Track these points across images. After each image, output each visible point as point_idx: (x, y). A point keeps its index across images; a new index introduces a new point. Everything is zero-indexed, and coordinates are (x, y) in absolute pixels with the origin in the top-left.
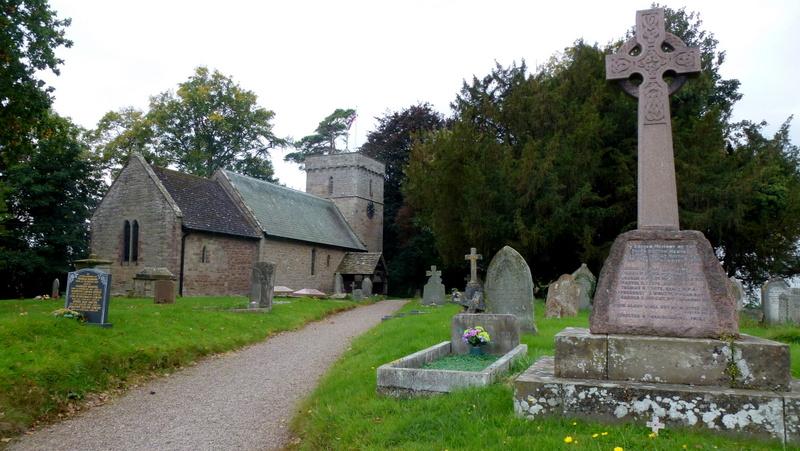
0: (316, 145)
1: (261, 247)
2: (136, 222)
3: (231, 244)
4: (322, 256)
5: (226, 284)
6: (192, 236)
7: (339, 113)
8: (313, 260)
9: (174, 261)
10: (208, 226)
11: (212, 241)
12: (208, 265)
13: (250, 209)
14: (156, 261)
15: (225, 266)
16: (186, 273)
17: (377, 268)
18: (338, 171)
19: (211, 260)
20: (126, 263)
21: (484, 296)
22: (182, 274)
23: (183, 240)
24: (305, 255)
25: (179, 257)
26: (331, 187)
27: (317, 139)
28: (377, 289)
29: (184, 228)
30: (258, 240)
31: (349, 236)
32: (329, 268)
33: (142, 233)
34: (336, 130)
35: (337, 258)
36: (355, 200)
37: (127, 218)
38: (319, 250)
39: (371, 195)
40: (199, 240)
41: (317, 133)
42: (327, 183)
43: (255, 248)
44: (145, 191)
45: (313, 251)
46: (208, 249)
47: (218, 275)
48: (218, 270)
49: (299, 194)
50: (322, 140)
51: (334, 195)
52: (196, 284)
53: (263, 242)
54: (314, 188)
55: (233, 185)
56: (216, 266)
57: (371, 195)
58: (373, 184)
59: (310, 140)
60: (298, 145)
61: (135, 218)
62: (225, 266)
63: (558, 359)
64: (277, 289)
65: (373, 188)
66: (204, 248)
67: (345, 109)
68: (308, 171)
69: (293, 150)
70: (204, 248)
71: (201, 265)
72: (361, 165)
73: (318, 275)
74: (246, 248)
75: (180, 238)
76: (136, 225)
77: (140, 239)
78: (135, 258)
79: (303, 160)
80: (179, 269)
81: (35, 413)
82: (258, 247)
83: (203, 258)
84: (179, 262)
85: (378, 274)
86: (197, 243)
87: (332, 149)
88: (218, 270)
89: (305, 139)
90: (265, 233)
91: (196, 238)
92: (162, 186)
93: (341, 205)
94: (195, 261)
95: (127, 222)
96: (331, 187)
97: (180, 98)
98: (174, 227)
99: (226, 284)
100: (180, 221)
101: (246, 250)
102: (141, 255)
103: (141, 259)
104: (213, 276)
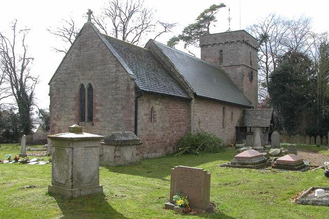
1: (192, 105)
6: (143, 97)
7: (214, 8)
8: (224, 112)
11: (157, 102)
15: (167, 125)
21: (114, 24)
25: (133, 119)
26: (221, 59)
27: (198, 26)
37: (82, 82)
40: (148, 101)
42: (218, 55)
45: (224, 109)
46: (155, 110)
47: (162, 133)
48: (162, 128)
52: (147, 142)
57: (251, 65)
61: (89, 82)
62: (167, 125)
63: (32, 138)
74: (181, 108)
75: (133, 100)
76: (90, 88)
77: (96, 100)
78: (91, 119)
83: (152, 117)
84: (133, 123)
86: (147, 105)
90: (195, 94)
94: (146, 121)
95: (82, 86)
101: (181, 110)
102: (97, 116)
103: (97, 120)
104: (159, 134)
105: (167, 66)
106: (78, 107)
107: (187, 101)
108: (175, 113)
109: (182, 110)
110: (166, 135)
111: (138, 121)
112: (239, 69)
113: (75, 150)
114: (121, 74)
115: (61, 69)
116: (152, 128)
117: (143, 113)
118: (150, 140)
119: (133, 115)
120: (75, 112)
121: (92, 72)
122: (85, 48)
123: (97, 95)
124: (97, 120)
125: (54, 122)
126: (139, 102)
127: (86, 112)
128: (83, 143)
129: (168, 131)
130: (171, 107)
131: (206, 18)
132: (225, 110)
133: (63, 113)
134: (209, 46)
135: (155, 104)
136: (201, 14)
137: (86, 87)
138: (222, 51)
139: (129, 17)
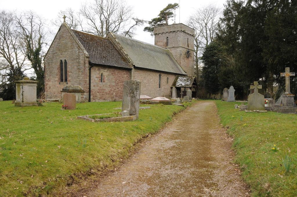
0: (159, 23)
2: (65, 60)
3: (116, 72)
4: (164, 77)
5: (114, 94)
6: (94, 68)
7: (171, 6)
8: (160, 80)
9: (86, 82)
10: (103, 62)
12: (104, 83)
13: (126, 53)
14: (75, 80)
16: (92, 88)
17: (193, 84)
18: (171, 34)
19: (105, 81)
20: (62, 83)
21: (101, 19)
22: (90, 89)
23: (90, 70)
24: (155, 77)
25: (88, 80)
26: (167, 44)
27: (159, 20)
28: (194, 95)
29: (90, 63)
30: (131, 69)
31: (177, 67)
32: (167, 82)
33: (69, 66)
34: (168, 15)
35: (172, 79)
36: (181, 49)
37: (61, 59)
38: (163, 75)
39: (188, 46)
40: (99, 70)
41: (159, 17)
42: (165, 41)
43: (129, 73)
44: (69, 44)
45: (160, 75)
46: (104, 75)
48: (110, 86)
49: (150, 46)
50: (162, 20)
51: (169, 46)
52: (98, 94)
53: (133, 70)
54: (159, 43)
55: (117, 41)
56: (109, 84)
57: (188, 46)
58: (189, 40)
59: (155, 20)
60: (150, 23)
61: (65, 58)
62: (114, 84)
64: (142, 97)
65: (189, 42)
66: (102, 74)
67: (173, 4)
68: (156, 34)
69: (148, 25)
70: (102, 74)
71: (101, 83)
72: (183, 30)
73: (163, 87)
74: (124, 74)
75: (88, 69)
77: (68, 69)
78: (66, 80)
79: (152, 31)
80: (88, 86)
81: (163, 146)
82: (131, 73)
83: (102, 80)
84: (88, 82)
85: (194, 87)
86: (98, 72)
87: (167, 24)
88: (110, 86)
89: (154, 20)
90: (134, 66)
91: (97, 69)
92: (78, 40)
93: (173, 52)
95: (61, 61)
96: (167, 44)
97: (169, 142)
98: (85, 63)
99: (114, 94)
100: (88, 59)
101: (124, 75)
102: (69, 78)
103: (70, 81)
104: (107, 90)
105: (118, 49)
106: (59, 74)
107: (129, 70)
108: (119, 77)
109: (126, 76)
110: (113, 90)
111: (91, 81)
112: (179, 49)
113: (24, 87)
114: (81, 54)
115: (50, 51)
116: (102, 85)
117: (95, 76)
118: (101, 92)
119: (88, 78)
120: (58, 76)
121: (66, 53)
122: (62, 39)
123: (69, 66)
124: (70, 81)
125: (47, 82)
126: (92, 70)
127: (64, 77)
128: (28, 84)
129: (114, 88)
130: (117, 73)
131: (165, 15)
132: (161, 76)
133: (51, 77)
134: (160, 35)
135: (104, 71)
136: (161, 11)
137: (63, 62)
138: (168, 38)
139: (110, 14)
